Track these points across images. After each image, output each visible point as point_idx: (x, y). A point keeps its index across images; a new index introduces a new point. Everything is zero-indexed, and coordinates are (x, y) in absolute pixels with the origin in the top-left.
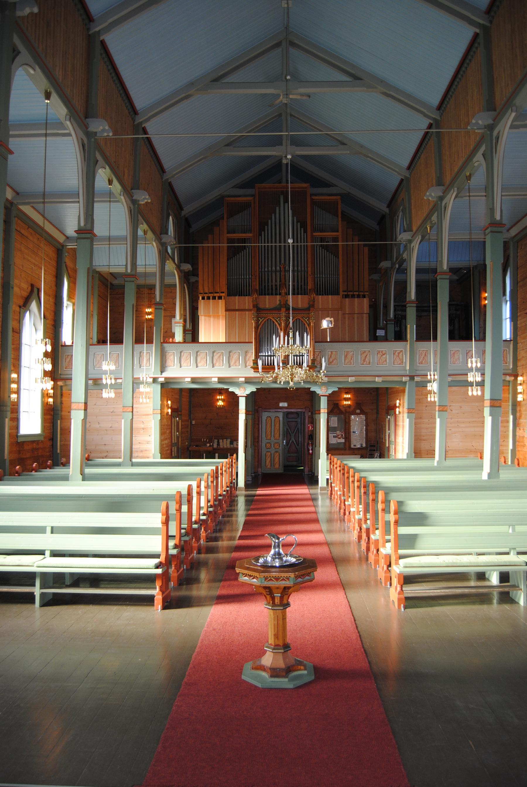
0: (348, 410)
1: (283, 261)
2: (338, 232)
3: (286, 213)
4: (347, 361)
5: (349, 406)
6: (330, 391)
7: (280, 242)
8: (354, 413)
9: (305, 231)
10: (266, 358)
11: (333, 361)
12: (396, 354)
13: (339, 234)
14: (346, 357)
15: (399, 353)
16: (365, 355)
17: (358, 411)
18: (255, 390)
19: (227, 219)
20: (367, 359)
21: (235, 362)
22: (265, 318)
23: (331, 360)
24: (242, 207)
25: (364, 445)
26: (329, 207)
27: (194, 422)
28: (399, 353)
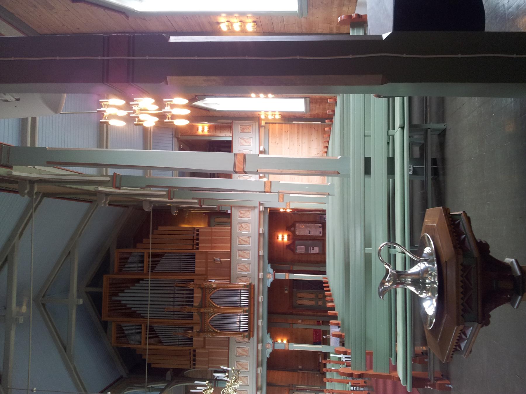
0: (291, 237)
1: (163, 310)
2: (144, 253)
3: (127, 297)
4: (247, 257)
5: (288, 236)
6: (271, 271)
7: (147, 308)
8: (294, 232)
9: (142, 280)
10: (242, 325)
12: (241, 215)
13: (145, 251)
15: (241, 214)
16: (242, 241)
17: (293, 229)
18: (269, 335)
19: (129, 344)
20: (245, 240)
21: (245, 351)
22: (208, 326)
23: (245, 269)
24: (120, 330)
25: (320, 225)
26: (124, 259)
27: (300, 367)
28: (241, 214)
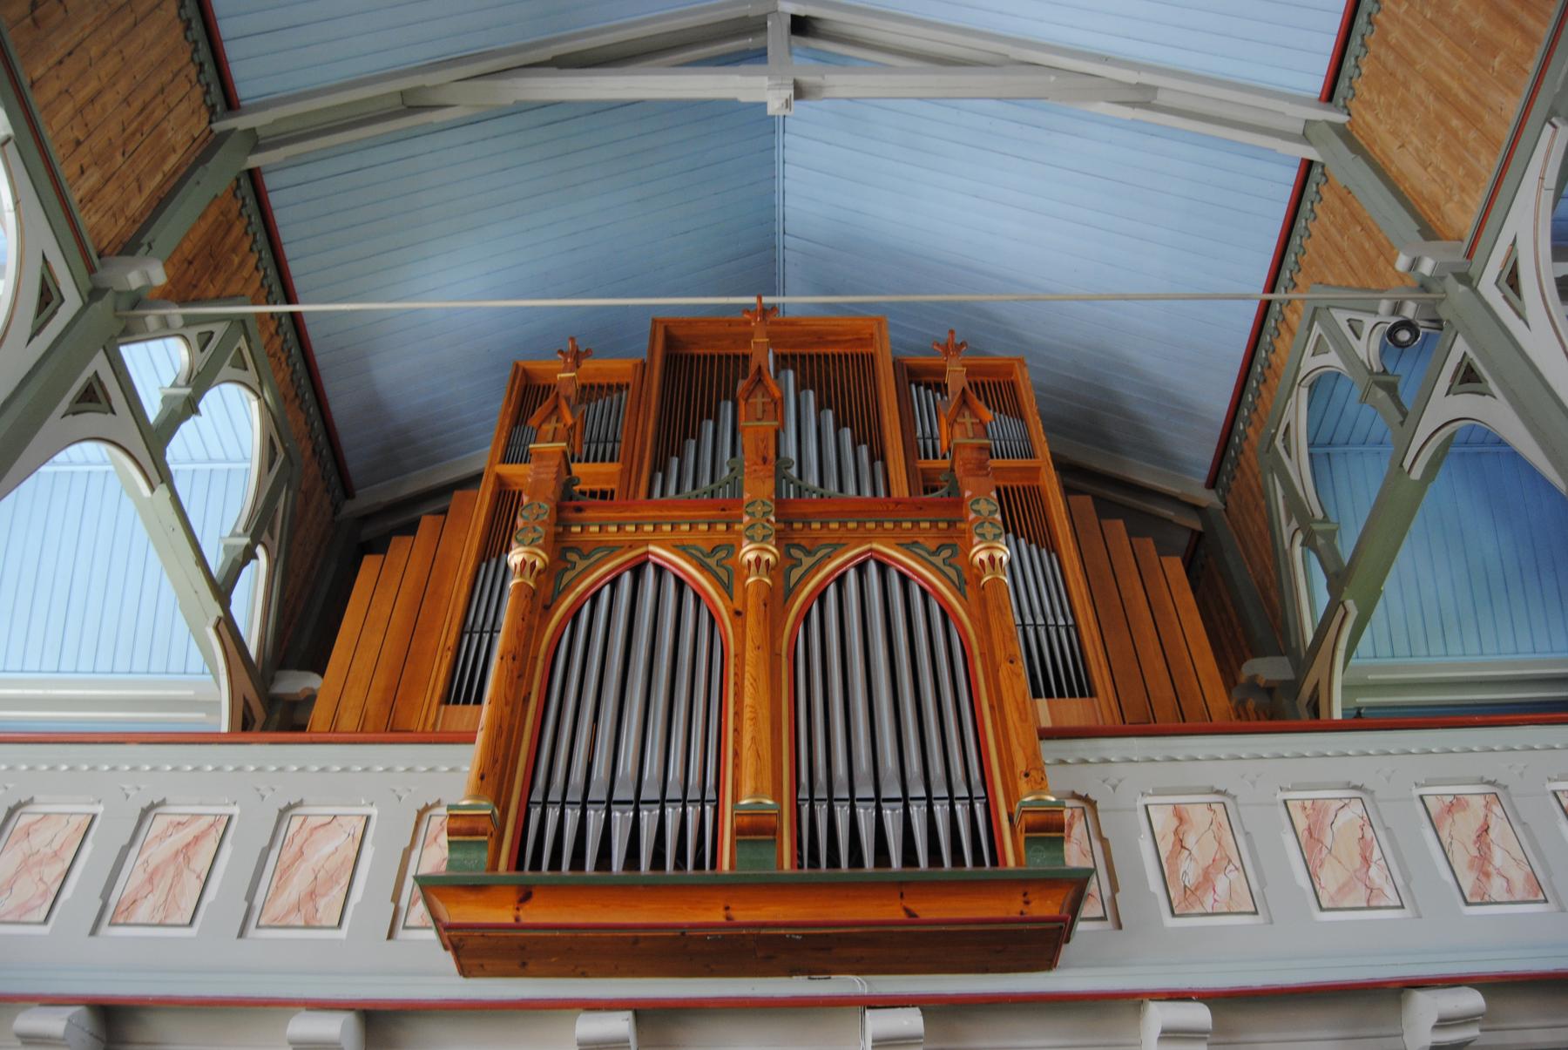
4: (1330, 879)
11: (1207, 880)
14: (1311, 843)
23: (1189, 870)
